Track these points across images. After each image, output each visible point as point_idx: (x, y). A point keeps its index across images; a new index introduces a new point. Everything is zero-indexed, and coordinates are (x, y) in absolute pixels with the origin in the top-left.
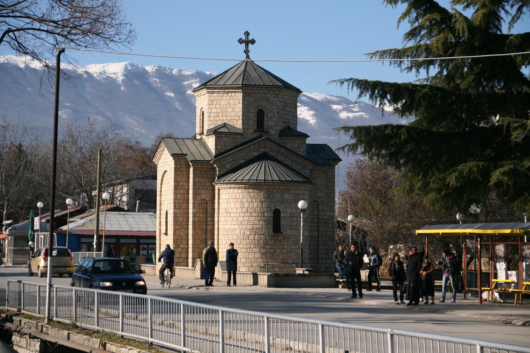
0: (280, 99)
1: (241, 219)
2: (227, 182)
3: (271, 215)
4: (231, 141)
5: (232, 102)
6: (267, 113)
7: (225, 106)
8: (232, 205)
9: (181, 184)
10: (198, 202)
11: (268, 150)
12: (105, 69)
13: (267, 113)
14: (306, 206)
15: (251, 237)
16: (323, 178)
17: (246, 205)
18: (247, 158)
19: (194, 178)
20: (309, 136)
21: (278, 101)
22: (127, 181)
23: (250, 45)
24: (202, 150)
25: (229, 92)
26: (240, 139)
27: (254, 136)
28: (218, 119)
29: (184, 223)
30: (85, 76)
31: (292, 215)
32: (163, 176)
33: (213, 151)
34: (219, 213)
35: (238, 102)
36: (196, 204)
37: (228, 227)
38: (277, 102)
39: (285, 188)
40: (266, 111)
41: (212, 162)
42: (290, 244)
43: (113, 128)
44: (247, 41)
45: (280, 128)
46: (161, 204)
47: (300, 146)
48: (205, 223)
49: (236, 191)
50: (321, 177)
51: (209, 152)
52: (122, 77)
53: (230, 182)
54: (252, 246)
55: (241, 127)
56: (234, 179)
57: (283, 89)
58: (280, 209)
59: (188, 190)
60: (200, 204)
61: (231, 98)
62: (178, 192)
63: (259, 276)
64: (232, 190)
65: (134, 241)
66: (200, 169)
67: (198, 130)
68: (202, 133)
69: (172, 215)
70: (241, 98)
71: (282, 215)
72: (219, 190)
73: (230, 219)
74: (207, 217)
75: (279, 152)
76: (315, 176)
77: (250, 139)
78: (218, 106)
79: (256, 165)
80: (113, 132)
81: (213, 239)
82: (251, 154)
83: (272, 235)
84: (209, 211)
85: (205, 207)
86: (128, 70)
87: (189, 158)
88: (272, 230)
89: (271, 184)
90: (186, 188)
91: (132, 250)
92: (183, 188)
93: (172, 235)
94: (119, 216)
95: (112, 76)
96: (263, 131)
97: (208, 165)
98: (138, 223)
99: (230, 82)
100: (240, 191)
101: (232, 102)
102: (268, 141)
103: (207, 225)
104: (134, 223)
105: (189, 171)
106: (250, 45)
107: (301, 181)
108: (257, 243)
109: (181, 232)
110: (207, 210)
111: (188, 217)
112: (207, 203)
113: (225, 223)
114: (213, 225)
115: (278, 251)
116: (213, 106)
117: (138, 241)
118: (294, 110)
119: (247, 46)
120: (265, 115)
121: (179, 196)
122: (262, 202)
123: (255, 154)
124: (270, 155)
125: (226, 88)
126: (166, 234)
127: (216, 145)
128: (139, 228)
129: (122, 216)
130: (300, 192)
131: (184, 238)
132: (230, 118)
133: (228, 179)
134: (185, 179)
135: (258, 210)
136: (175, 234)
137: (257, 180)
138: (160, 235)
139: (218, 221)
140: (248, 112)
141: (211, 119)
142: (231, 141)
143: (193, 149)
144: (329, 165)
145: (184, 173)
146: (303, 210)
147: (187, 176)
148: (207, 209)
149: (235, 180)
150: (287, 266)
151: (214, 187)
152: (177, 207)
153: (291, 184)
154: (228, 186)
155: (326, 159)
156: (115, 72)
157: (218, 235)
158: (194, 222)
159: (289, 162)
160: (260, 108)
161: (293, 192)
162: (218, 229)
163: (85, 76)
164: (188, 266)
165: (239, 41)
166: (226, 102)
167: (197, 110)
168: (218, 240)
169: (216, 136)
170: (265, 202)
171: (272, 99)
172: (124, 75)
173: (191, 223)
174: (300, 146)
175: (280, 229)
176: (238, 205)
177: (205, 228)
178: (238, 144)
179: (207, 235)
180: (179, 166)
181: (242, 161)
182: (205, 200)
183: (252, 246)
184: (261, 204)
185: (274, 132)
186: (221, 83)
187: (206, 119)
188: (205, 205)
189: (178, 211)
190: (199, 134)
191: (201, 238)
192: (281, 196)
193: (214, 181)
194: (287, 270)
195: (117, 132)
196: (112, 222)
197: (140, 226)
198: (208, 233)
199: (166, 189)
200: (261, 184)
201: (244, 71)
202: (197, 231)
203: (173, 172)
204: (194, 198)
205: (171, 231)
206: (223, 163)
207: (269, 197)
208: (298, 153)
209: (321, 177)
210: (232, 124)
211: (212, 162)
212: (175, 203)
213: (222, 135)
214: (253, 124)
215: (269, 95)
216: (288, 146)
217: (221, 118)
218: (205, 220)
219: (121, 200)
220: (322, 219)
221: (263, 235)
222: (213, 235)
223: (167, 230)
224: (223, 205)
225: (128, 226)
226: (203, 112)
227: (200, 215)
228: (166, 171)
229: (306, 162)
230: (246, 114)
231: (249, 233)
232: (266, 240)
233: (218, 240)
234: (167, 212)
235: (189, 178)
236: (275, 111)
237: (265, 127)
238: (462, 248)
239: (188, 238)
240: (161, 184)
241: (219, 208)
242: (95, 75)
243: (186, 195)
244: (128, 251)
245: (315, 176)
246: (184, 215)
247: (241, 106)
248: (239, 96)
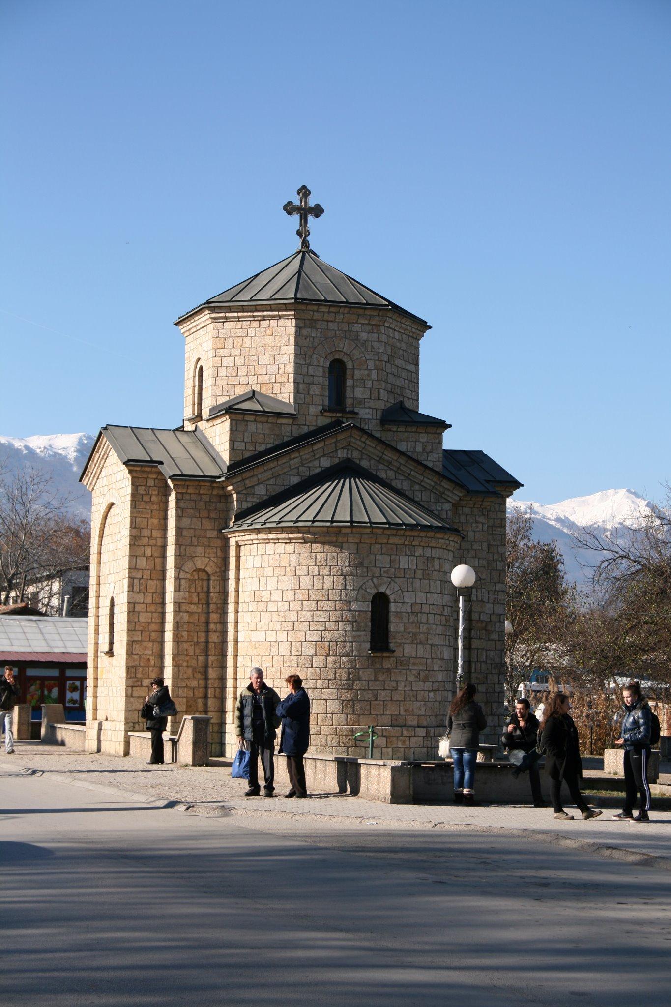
0: (384, 338)
1: (292, 616)
2: (258, 526)
3: (367, 607)
4: (267, 432)
5: (269, 340)
6: (353, 369)
7: (253, 352)
8: (272, 584)
9: (146, 533)
10: (188, 576)
11: (356, 454)
12: (51, 442)
13: (353, 369)
14: (471, 581)
15: (318, 661)
16: (480, 526)
17: (306, 582)
18: (306, 473)
19: (179, 517)
20: (450, 426)
21: (379, 341)
22: (60, 574)
23: (310, 218)
24: (199, 454)
25: (264, 318)
26: (288, 428)
27: (323, 421)
29: (153, 627)
30: (25, 452)
31: (417, 608)
32: (105, 518)
33: (225, 457)
34: (237, 603)
35: (284, 340)
36: (183, 582)
37: (259, 636)
38: (375, 344)
39: (400, 542)
40: (349, 365)
41: (223, 479)
42: (411, 678)
43: (36, 481)
44: (305, 210)
45: (381, 405)
46: (99, 584)
47: (429, 448)
48: (203, 628)
49: (280, 547)
50: (477, 522)
51: (214, 459)
52: (75, 454)
53: (268, 525)
54: (319, 683)
55: (292, 401)
56: (276, 518)
57: (390, 314)
58: (388, 592)
59: (164, 547)
60: (191, 581)
61: (269, 332)
62: (140, 551)
63: (363, 770)
64: (270, 546)
65: (55, 673)
66: (193, 497)
67: (188, 411)
68: (199, 418)
69: (125, 608)
70: (292, 331)
71: (393, 607)
72: (238, 546)
73: (265, 617)
74: (208, 613)
75: (380, 461)
76: (462, 519)
77: (312, 428)
78: (236, 352)
79: (328, 487)
80: (36, 487)
81: (223, 667)
82: (316, 463)
83: (369, 657)
85: (205, 589)
86: (83, 444)
87: (168, 470)
88: (368, 645)
89: (368, 530)
90: (160, 542)
91: (50, 691)
92: (152, 542)
93: (125, 657)
94: (26, 624)
95: (61, 452)
96: (343, 411)
97: (213, 488)
98: (64, 637)
99: (266, 295)
100: (290, 548)
101: (269, 340)
102: (356, 434)
103: (207, 632)
104: (57, 637)
105: (166, 502)
106: (310, 218)
107: (430, 527)
108: (331, 676)
109: (146, 648)
110: (208, 597)
111: (163, 613)
112: (209, 580)
113: (252, 626)
114: (224, 633)
115: (383, 695)
116: (225, 352)
117: (63, 672)
118: (411, 368)
119: (304, 219)
120: (348, 372)
121: (142, 562)
122: (344, 576)
123: (326, 463)
124: (359, 465)
125: (256, 309)
126: (110, 653)
127: (232, 441)
128: (66, 647)
129: (33, 624)
130: (434, 553)
131: (152, 663)
132: (266, 379)
133: (263, 519)
134: (156, 521)
135: (334, 595)
136: (130, 654)
137: (332, 522)
138: (96, 656)
139: (236, 623)
140: (309, 365)
142: (267, 432)
143: (176, 450)
144: (495, 494)
145: (155, 507)
146: (466, 591)
147: (162, 513)
149: (280, 522)
150: (405, 733)
151: (226, 540)
152: (136, 589)
153: (416, 534)
154: (260, 537)
155: (488, 482)
156: (65, 446)
157: (236, 656)
158: (177, 625)
159: (405, 483)
160: (337, 357)
161: (419, 552)
162: (236, 642)
163: (25, 452)
165: (285, 208)
166: (257, 342)
167: (187, 367)
168: (236, 668)
169: (231, 420)
170: (351, 574)
171: (364, 336)
172: (78, 451)
173: (169, 626)
174: (429, 448)
175: (388, 643)
176: (286, 583)
177: (203, 640)
178: (286, 439)
179: (207, 656)
180: (141, 490)
181: (295, 480)
182: (204, 570)
183: (319, 683)
184: (341, 579)
185: (368, 414)
186: (246, 296)
187: (208, 382)
188: (205, 584)
189: (140, 598)
190: (189, 420)
191: (193, 663)
192: (392, 562)
193: (227, 527)
194: (404, 742)
195: (41, 487)
196: (12, 636)
197: (69, 644)
198: (212, 651)
199: (112, 547)
200: (344, 531)
201: (299, 273)
202: (185, 646)
203: (128, 505)
204: (178, 567)
205: (121, 647)
206: (248, 483)
207: (361, 564)
208: (425, 463)
209: (477, 522)
210: (269, 393)
211: (223, 479)
212: (131, 578)
213: (247, 418)
214: (320, 394)
215: (357, 327)
216: (402, 447)
217: (244, 380)
218: (203, 619)
219: (49, 603)
220: (479, 621)
221: (347, 655)
222: (223, 655)
223: (111, 643)
224: (249, 583)
225: (43, 643)
226: (201, 368)
227: (193, 608)
228: (112, 505)
229: (445, 484)
230: (305, 370)
231: (312, 652)
232: (354, 668)
233: (236, 668)
234: (112, 600)
235: (165, 518)
236: (371, 365)
237: (349, 402)
239: (162, 662)
240: (101, 537)
241: (237, 591)
242: (38, 451)
243: (158, 560)
244: (43, 692)
245: (462, 519)
246: (153, 608)
247: (291, 349)
248: (287, 327)
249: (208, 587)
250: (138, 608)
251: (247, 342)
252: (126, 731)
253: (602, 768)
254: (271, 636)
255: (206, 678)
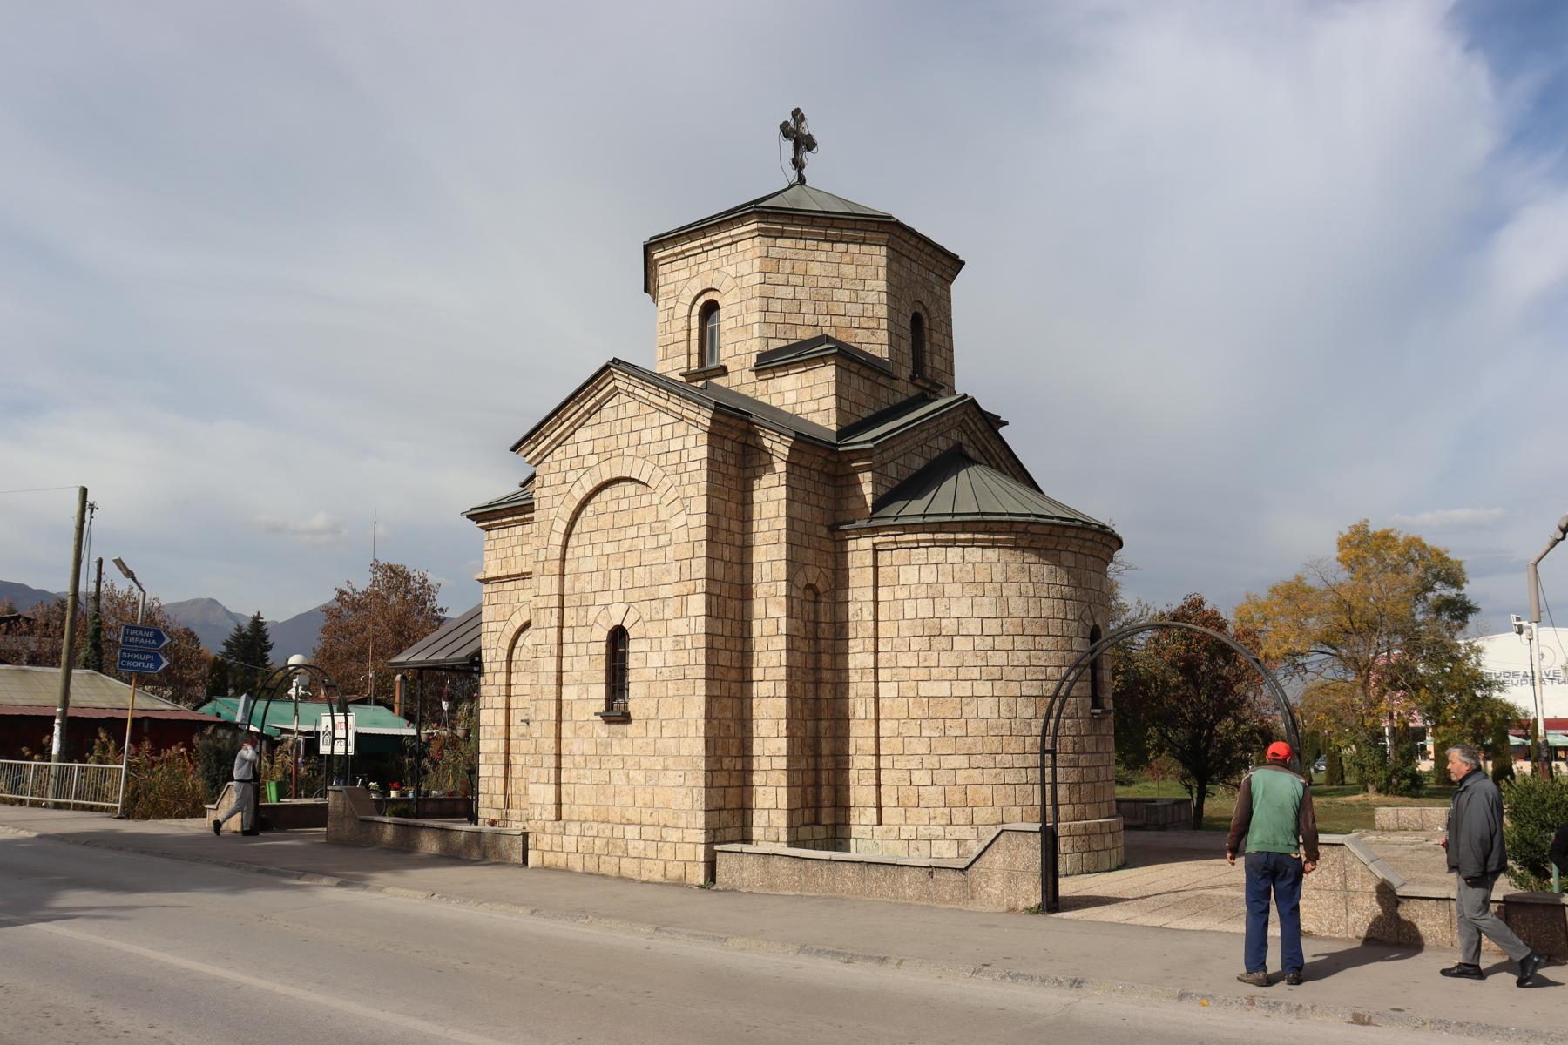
1: (999, 658)
17: (1017, 606)
20: (1006, 423)
28: (798, 320)
35: (871, 272)
44: (799, 138)
49: (974, 554)
61: (847, 259)
73: (948, 659)
84: (826, 630)
100: (992, 554)
101: (849, 270)
121: (720, 571)
132: (845, 321)
141: (771, 318)
148: (817, 622)
149: (897, 518)
164: (747, 840)
176: (986, 607)
177: (811, 695)
217: (809, 319)
231: (1030, 713)
237: (928, 371)
238: (393, 684)
249: (816, 612)
250: (718, 642)
251: (814, 268)
252: (709, 844)
253: (848, 850)
254: (964, 689)
255: (817, 755)
